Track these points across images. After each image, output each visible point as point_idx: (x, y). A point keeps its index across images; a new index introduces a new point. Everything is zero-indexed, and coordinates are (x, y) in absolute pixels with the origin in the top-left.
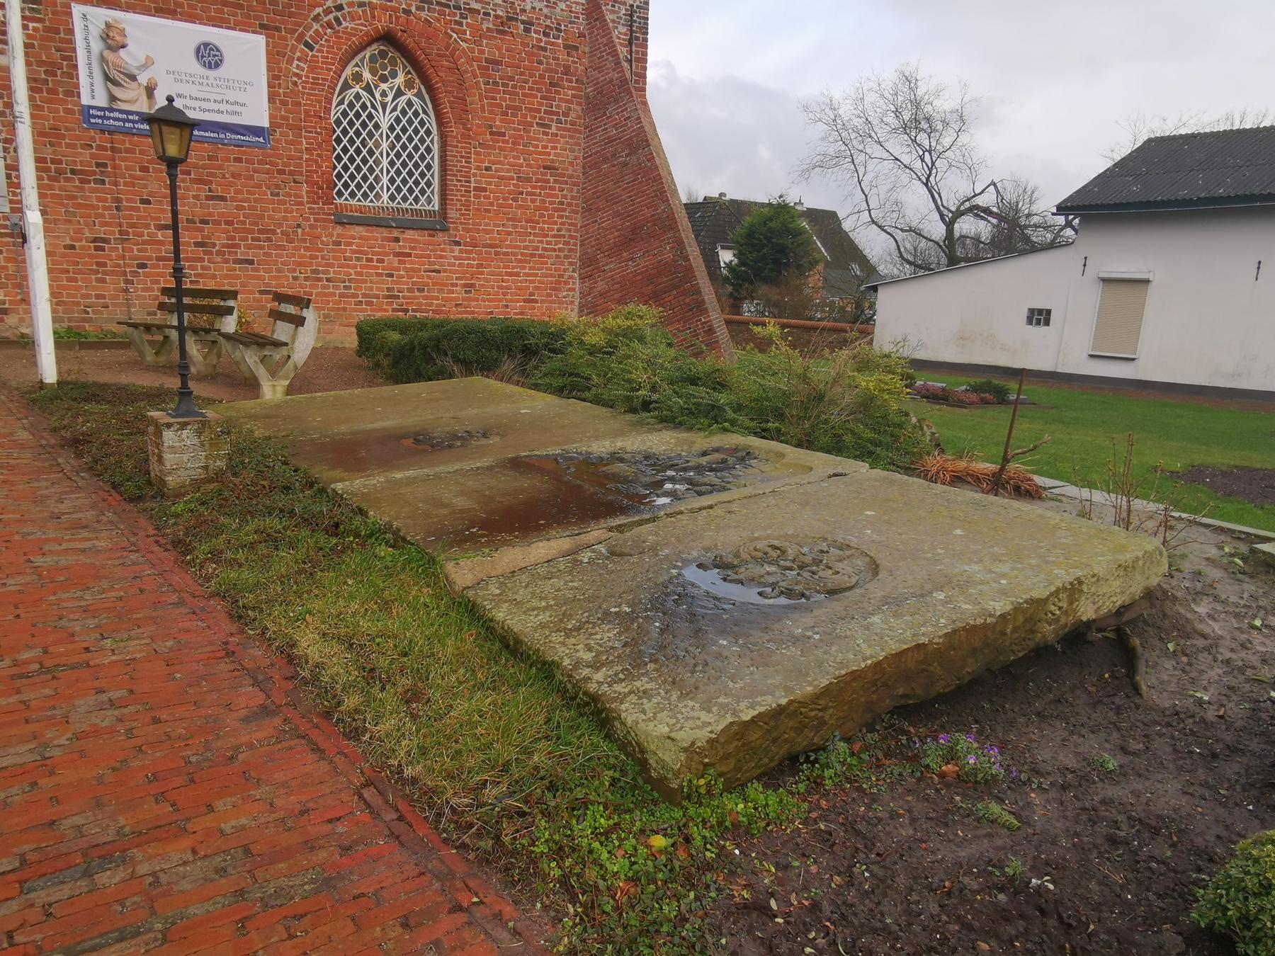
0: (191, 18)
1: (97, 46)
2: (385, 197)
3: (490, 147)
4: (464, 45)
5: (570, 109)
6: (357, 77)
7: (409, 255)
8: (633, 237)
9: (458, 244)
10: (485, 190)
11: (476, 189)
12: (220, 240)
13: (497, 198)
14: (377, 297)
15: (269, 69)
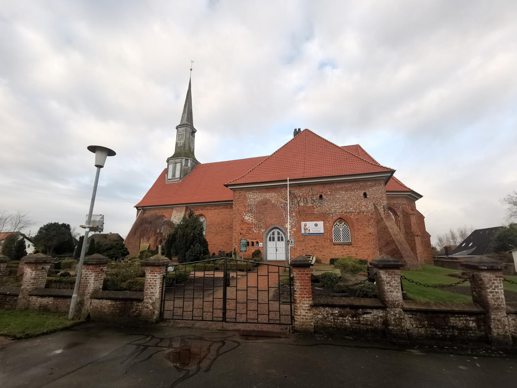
8: (387, 244)
12: (317, 248)
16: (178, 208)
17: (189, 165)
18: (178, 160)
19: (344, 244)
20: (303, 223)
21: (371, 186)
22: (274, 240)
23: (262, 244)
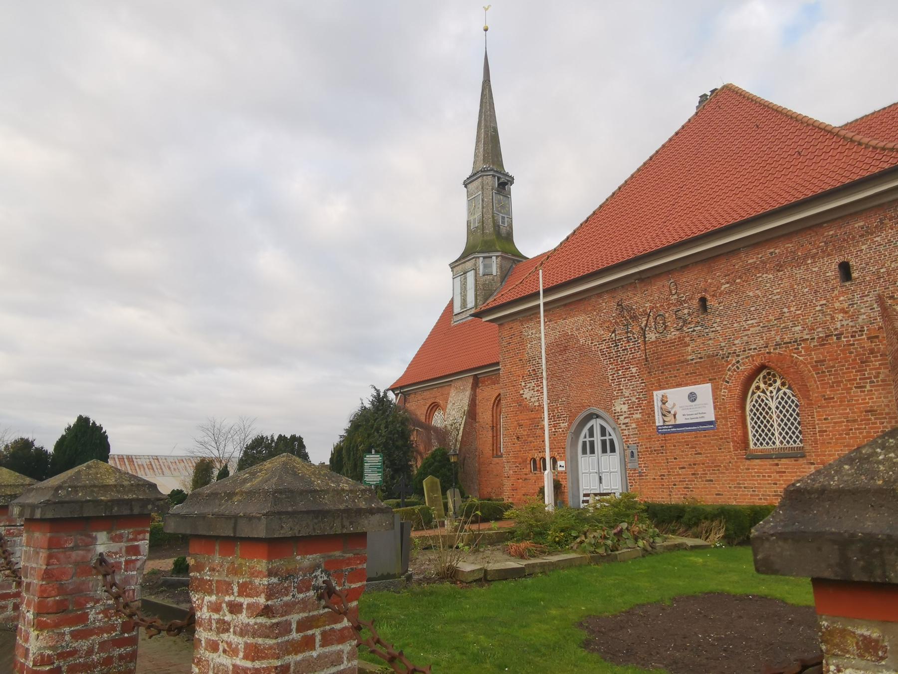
0: (686, 385)
1: (660, 404)
2: (778, 442)
3: (824, 407)
4: (801, 358)
5: (879, 373)
6: (758, 388)
7: (785, 472)
9: (812, 464)
10: (826, 431)
11: (819, 432)
13: (835, 435)
14: (769, 495)
15: (713, 396)
16: (459, 383)
17: (495, 270)
18: (469, 265)
19: (781, 455)
20: (657, 395)
21: (868, 232)
22: (592, 451)
23: (562, 463)
